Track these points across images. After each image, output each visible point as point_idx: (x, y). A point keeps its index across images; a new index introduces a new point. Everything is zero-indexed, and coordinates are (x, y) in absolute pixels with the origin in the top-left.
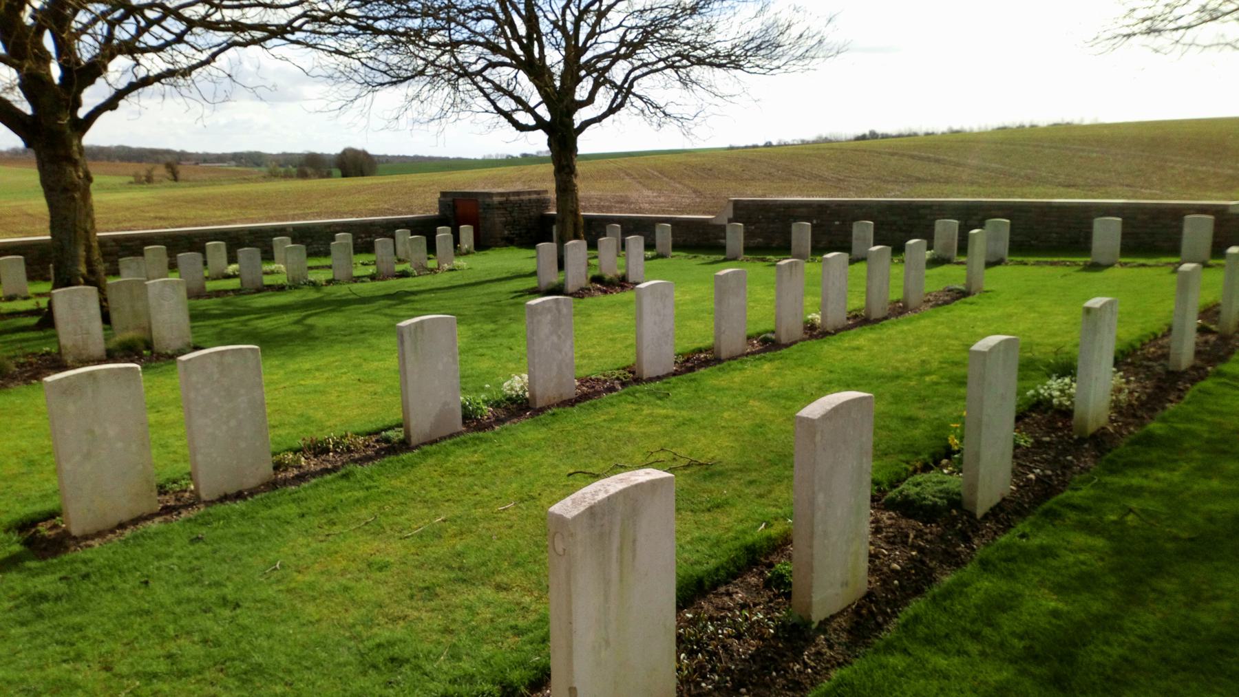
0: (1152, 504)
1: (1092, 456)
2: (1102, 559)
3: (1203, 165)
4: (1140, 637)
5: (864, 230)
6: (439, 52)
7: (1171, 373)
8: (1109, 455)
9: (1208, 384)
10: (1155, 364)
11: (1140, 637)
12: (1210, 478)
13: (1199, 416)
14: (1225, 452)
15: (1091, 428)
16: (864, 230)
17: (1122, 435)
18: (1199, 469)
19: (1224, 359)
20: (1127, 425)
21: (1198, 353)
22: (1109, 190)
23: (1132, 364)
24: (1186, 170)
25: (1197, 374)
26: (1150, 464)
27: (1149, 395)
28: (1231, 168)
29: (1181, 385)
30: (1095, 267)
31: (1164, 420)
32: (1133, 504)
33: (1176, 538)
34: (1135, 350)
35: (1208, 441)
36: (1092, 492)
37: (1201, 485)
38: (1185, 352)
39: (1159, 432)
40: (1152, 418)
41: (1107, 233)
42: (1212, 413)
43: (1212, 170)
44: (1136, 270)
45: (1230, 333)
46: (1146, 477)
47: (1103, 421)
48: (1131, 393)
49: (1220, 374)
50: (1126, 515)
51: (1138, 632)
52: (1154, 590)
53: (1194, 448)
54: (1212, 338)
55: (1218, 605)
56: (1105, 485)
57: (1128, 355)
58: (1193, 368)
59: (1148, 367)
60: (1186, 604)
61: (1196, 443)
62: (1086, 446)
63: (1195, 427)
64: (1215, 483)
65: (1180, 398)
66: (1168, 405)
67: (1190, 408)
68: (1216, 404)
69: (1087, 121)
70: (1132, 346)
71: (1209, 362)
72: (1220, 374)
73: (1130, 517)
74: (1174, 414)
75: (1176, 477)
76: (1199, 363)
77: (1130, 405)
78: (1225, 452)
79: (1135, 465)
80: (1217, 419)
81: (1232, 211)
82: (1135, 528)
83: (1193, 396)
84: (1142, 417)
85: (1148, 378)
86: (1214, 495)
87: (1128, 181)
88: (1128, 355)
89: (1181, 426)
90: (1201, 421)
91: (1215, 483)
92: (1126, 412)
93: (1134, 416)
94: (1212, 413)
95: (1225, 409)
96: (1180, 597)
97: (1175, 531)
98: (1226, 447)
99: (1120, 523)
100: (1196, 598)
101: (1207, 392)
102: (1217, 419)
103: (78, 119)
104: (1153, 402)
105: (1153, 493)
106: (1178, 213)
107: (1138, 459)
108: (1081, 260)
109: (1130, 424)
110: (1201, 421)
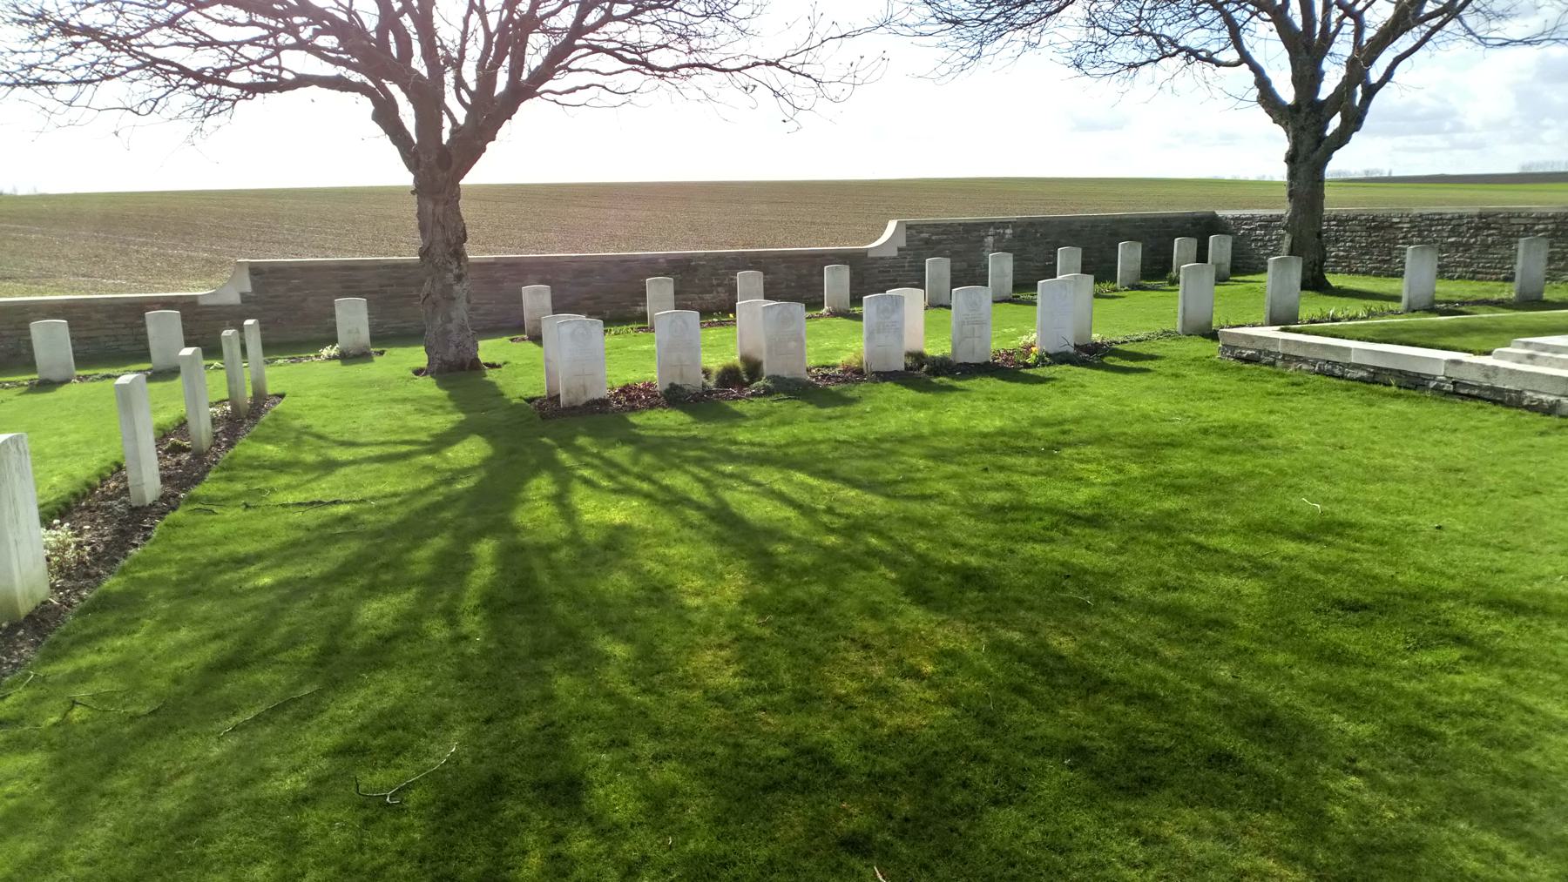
0: (103, 685)
1: (32, 645)
2: (38, 781)
3: (174, 247)
4: (85, 864)
5: (659, 291)
6: (493, 27)
7: (133, 510)
8: (52, 637)
9: (179, 514)
10: (114, 503)
11: (85, 864)
12: (178, 629)
13: (167, 556)
14: (196, 593)
15: (25, 608)
16: (659, 291)
17: (70, 605)
18: (165, 621)
19: (197, 481)
20: (76, 590)
21: (165, 480)
22: (60, 282)
23: (88, 508)
24: (153, 255)
25: (168, 503)
26: (104, 633)
27: (107, 544)
28: (205, 250)
29: (147, 523)
30: (46, 385)
31: (123, 572)
32: (82, 693)
33: (134, 718)
34: (93, 489)
35: (179, 584)
36: (25, 694)
37: (169, 640)
38: (148, 482)
39: (118, 588)
40: (110, 573)
41: (51, 342)
42: (181, 549)
43: (185, 254)
44: (99, 384)
45: (205, 448)
46: (99, 651)
47: (43, 591)
48: (79, 546)
49: (192, 499)
50: (72, 708)
51: (83, 858)
52: (103, 795)
53: (158, 597)
54: (185, 457)
55: (178, 783)
56: (44, 680)
57: (85, 496)
58: (163, 498)
59: (106, 508)
60: (143, 797)
61: (161, 591)
62: (21, 633)
63: (163, 570)
64: (184, 634)
65: (146, 538)
66: (132, 551)
67: (156, 549)
68: (187, 536)
69: (23, 190)
70: (88, 485)
71: (181, 488)
72: (192, 499)
73: (77, 710)
74: (138, 561)
75: (137, 640)
76: (169, 490)
77: (81, 562)
78: (196, 593)
79: (86, 640)
80: (188, 554)
81: (202, 302)
82: (84, 722)
83: (161, 534)
84: (99, 575)
85: (107, 522)
86: (183, 648)
87: (83, 270)
88: (85, 496)
89: (144, 574)
90: (169, 561)
91: (184, 634)
92: (69, 573)
93: (87, 575)
94: (181, 549)
95: (197, 541)
96: (139, 791)
97: (131, 710)
98: (197, 586)
99: (65, 722)
100: (155, 784)
101: (176, 525)
102: (188, 554)
103: (493, 100)
104: (110, 555)
105: (107, 669)
106: (139, 308)
107: (89, 631)
108: (24, 379)
109: (82, 587)
110: (169, 561)
